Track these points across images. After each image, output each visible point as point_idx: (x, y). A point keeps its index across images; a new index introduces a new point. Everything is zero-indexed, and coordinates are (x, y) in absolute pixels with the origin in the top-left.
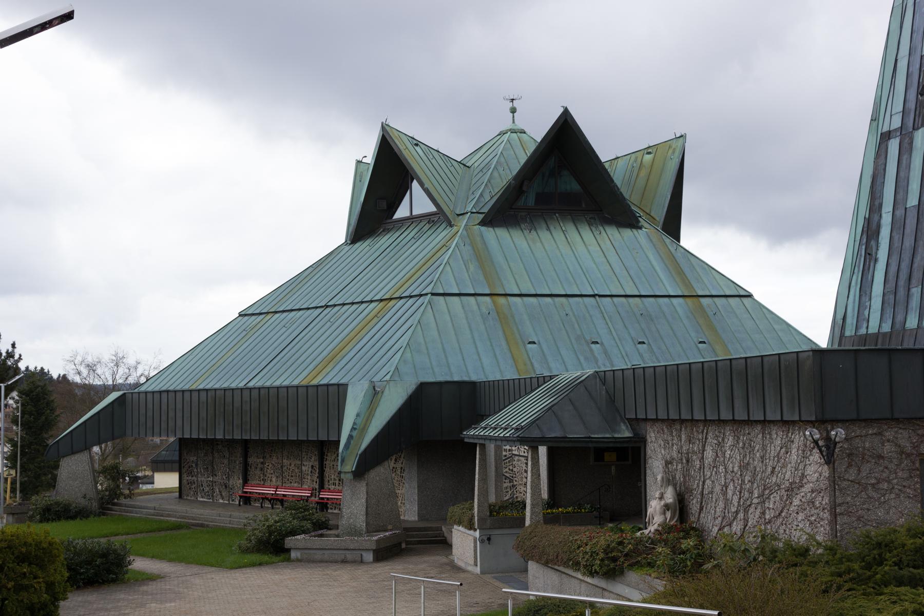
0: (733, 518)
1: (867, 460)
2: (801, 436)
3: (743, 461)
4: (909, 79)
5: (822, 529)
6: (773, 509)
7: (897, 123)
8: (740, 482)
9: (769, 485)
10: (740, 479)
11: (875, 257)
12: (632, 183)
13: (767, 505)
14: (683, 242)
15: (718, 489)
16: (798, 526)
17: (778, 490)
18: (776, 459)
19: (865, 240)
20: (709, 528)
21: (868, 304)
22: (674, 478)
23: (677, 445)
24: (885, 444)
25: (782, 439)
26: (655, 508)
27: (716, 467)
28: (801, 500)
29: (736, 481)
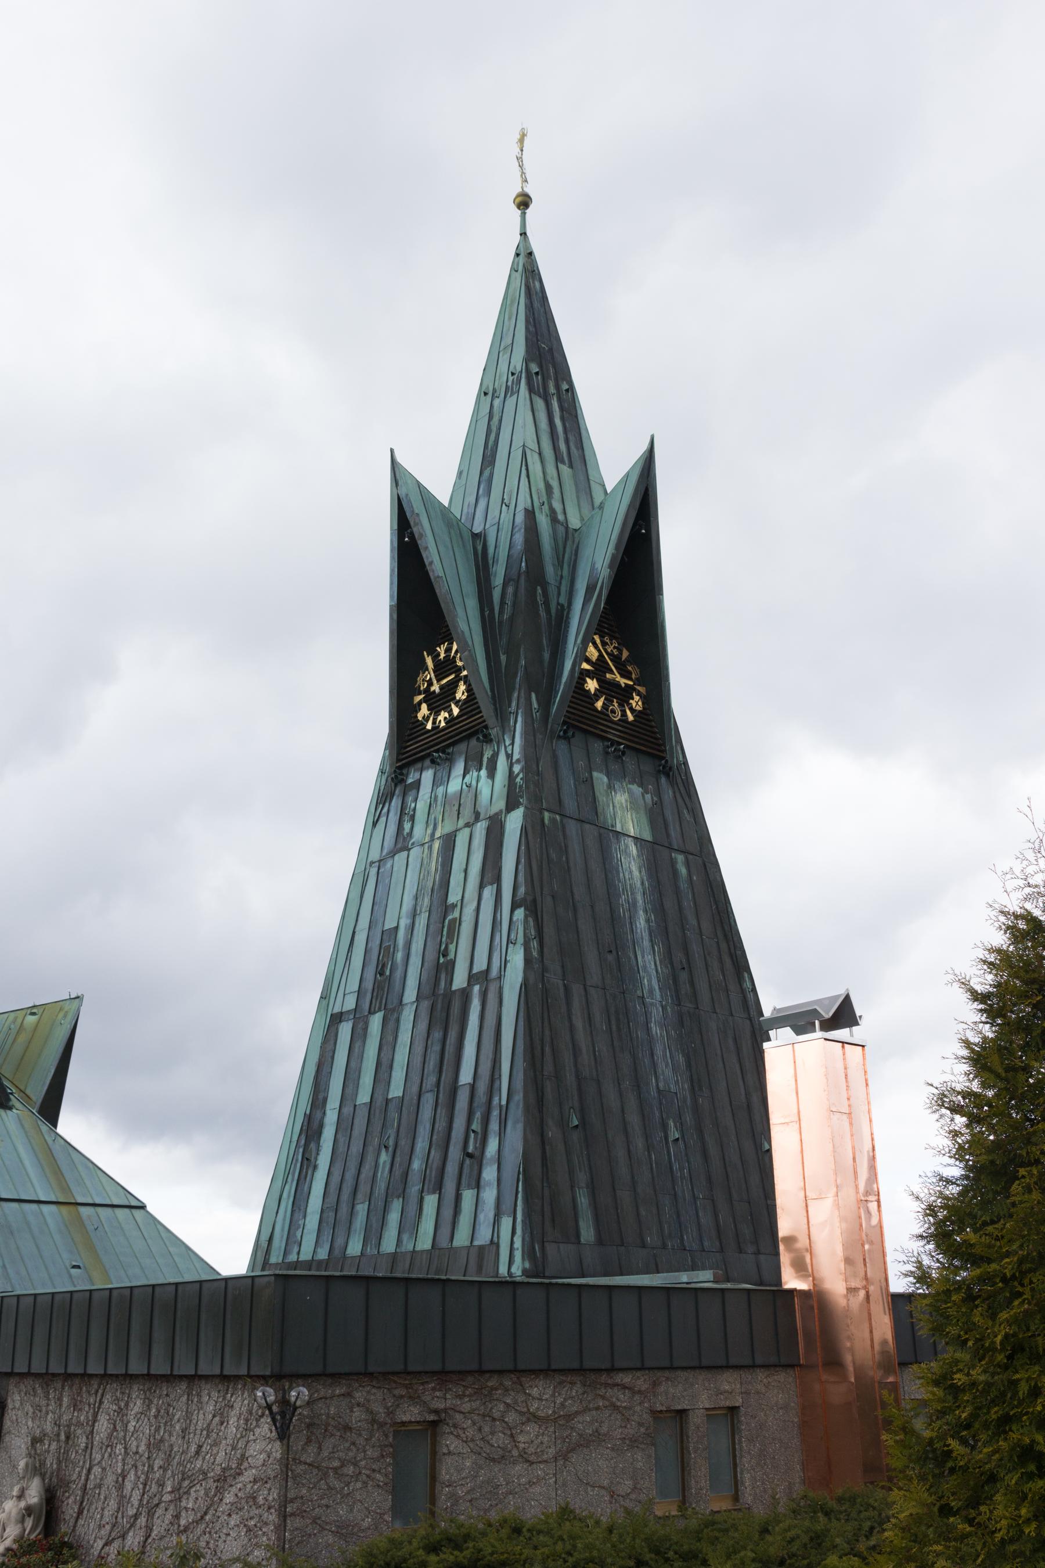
0: (129, 1525)
1: (331, 1433)
2: (246, 1399)
3: (155, 1436)
4: (367, 955)
5: (265, 1539)
6: (193, 1509)
7: (350, 1004)
8: (146, 1469)
9: (190, 1473)
10: (147, 1465)
11: (313, 1164)
12: (7, 1047)
13: (184, 1504)
14: (61, 1129)
15: (110, 1479)
16: (229, 1534)
17: (204, 1480)
18: (205, 1432)
19: (303, 1142)
20: (89, 1542)
21: (301, 1222)
22: (43, 1464)
23: (54, 1413)
24: (355, 1410)
25: (216, 1403)
26: (10, 1513)
27: (112, 1446)
28: (236, 1495)
29: (141, 1468)
